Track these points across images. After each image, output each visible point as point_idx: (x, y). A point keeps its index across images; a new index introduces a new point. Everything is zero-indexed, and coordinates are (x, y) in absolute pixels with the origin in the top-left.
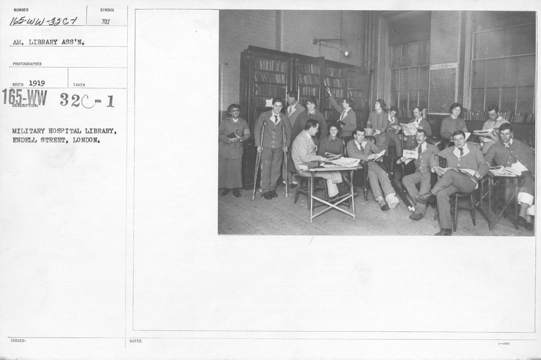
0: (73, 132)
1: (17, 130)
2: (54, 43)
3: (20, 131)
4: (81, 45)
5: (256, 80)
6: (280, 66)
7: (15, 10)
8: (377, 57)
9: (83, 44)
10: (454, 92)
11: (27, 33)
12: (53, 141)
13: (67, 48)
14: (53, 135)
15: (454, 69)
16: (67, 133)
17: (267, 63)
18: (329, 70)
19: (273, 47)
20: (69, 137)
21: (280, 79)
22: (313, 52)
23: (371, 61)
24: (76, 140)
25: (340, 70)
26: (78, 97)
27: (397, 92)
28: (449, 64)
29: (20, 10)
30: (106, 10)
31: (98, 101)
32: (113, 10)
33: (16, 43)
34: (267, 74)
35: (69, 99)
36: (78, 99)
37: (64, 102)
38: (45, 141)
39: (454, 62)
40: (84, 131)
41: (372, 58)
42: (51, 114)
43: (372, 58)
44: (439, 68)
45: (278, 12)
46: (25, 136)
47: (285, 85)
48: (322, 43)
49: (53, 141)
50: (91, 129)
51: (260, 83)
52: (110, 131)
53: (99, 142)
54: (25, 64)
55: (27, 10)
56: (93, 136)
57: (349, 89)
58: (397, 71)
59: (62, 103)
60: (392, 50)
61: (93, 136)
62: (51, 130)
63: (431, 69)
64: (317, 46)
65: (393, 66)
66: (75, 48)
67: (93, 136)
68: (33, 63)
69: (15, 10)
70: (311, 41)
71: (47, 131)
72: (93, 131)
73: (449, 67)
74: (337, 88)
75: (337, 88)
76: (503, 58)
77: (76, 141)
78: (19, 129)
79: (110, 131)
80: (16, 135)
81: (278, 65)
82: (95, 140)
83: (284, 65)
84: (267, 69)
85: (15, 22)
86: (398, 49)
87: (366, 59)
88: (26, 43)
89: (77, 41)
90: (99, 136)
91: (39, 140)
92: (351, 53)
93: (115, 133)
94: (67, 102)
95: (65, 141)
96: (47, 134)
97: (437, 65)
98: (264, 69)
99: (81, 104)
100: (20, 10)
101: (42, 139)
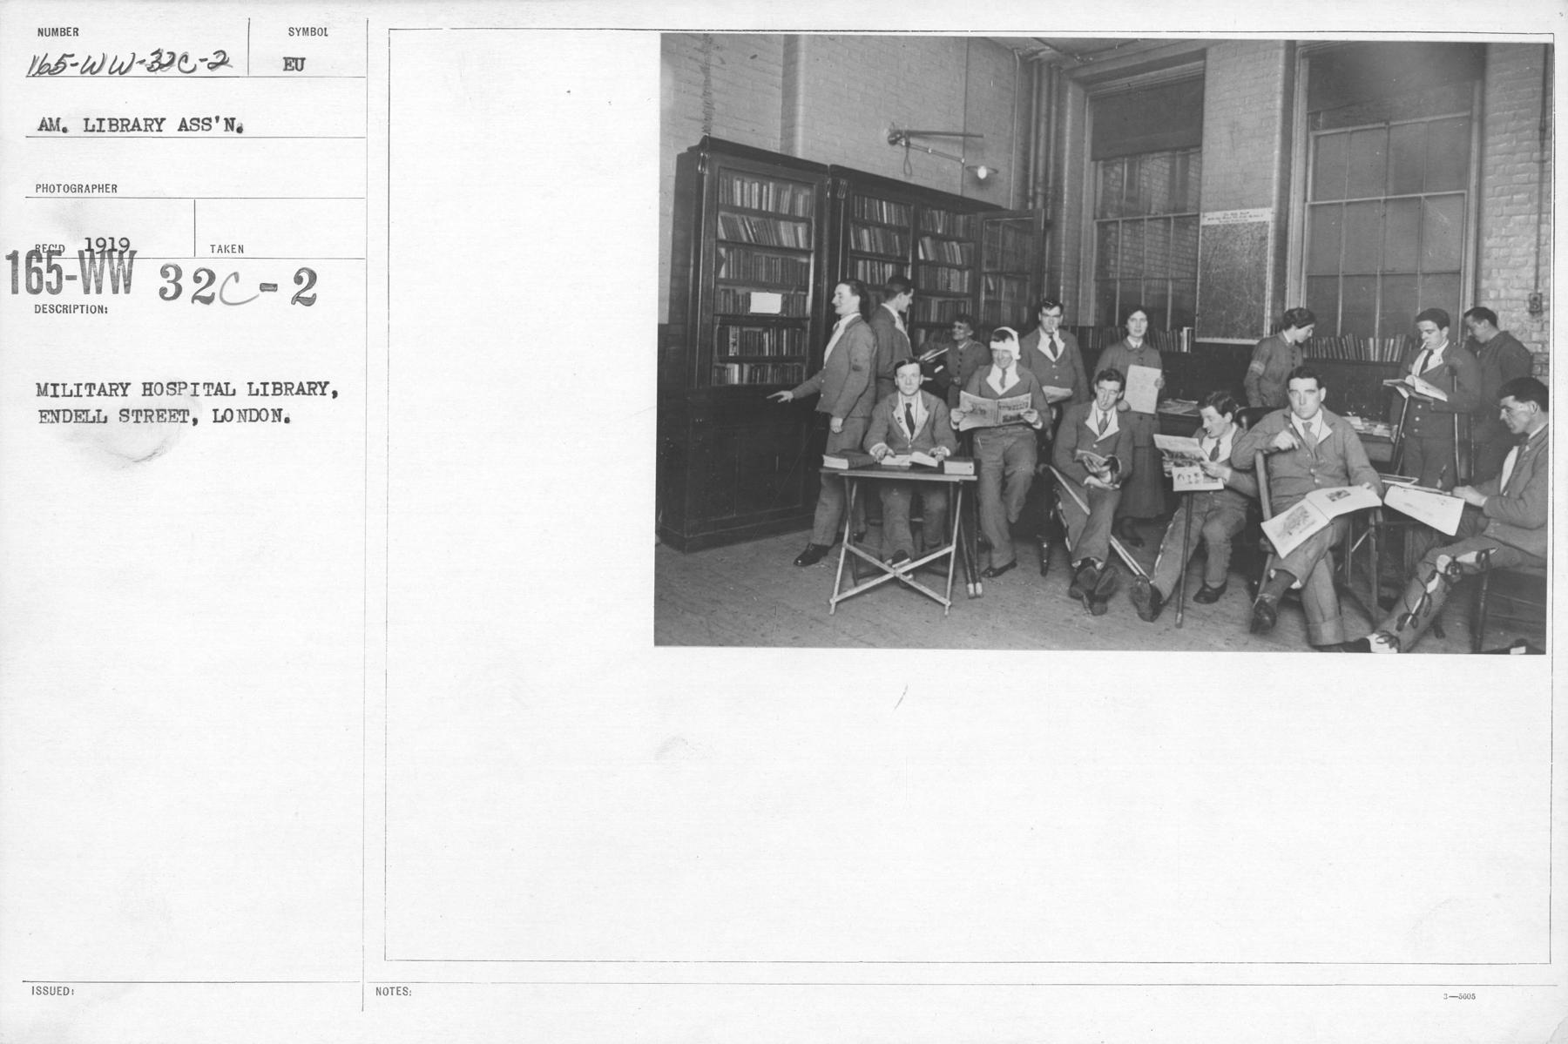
0: (212, 392)
1: (50, 390)
2: (155, 126)
3: (60, 390)
4: (235, 133)
5: (722, 235)
6: (794, 198)
7: (40, 32)
8: (1062, 188)
9: (240, 130)
10: (1262, 287)
11: (72, 97)
12: (155, 418)
13: (196, 143)
14: (154, 402)
15: (1264, 225)
16: (195, 394)
17: (756, 186)
18: (932, 217)
19: (774, 145)
20: (204, 406)
21: (791, 235)
22: (884, 162)
23: (1045, 197)
24: (220, 414)
25: (961, 218)
26: (212, 277)
27: (1115, 281)
28: (1252, 212)
29: (55, 32)
30: (306, 31)
31: (267, 287)
32: (324, 32)
33: (48, 126)
34: (754, 220)
35: (187, 282)
36: (210, 283)
37: (171, 291)
38: (133, 419)
39: (1263, 206)
40: (243, 390)
41: (1046, 188)
42: (137, 336)
43: (1046, 188)
44: (1223, 222)
45: (791, 42)
46: (73, 404)
47: (807, 253)
48: (913, 141)
49: (155, 418)
50: (265, 384)
51: (733, 243)
52: (319, 390)
53: (287, 421)
54: (68, 188)
55: (76, 31)
56: (271, 403)
57: (985, 269)
58: (1112, 228)
59: (163, 291)
60: (1100, 171)
61: (271, 402)
62: (148, 388)
63: (1204, 222)
64: (899, 150)
65: (1103, 215)
66: (217, 141)
67: (271, 402)
68: (94, 187)
69: (40, 32)
70: (885, 133)
71: (135, 391)
72: (270, 389)
73: (1250, 220)
74: (953, 266)
75: (953, 266)
76: (1386, 201)
77: (222, 418)
78: (55, 385)
79: (319, 390)
80: (48, 403)
81: (786, 196)
82: (277, 413)
83: (806, 198)
84: (755, 206)
85: (45, 69)
86: (1117, 169)
87: (1031, 193)
88: (76, 127)
89: (222, 122)
90: (288, 403)
91: (114, 417)
92: (996, 172)
93: (335, 394)
94: (179, 290)
95: (189, 419)
96: (135, 399)
97: (1219, 214)
98: (746, 205)
99: (217, 297)
100: (55, 32)
101: (124, 413)
